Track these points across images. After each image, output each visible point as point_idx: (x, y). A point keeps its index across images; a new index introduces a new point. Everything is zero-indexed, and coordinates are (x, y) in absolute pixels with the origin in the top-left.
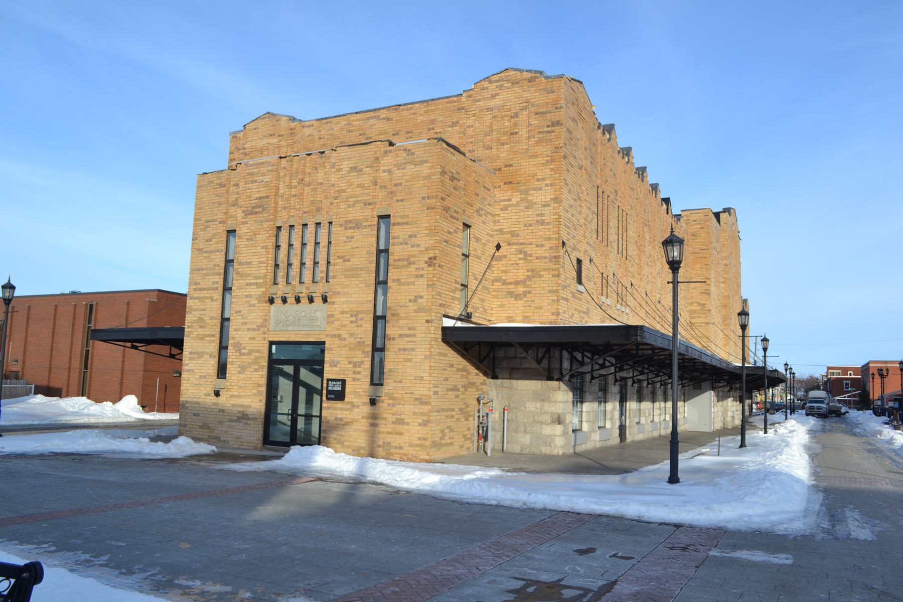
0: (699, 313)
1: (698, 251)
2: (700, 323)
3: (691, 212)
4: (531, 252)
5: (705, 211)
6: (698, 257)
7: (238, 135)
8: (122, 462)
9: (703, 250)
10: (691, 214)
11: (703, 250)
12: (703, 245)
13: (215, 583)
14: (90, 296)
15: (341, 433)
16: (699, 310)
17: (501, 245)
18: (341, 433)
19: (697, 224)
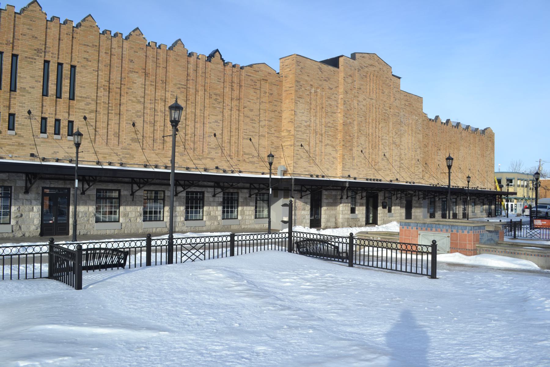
0: (287, 138)
1: (288, 89)
2: (287, 145)
3: (284, 59)
4: (23, 135)
5: (292, 56)
6: (287, 94)
7: (107, 32)
8: (77, 277)
9: (291, 87)
10: (285, 60)
11: (291, 87)
12: (290, 84)
13: (69, 241)
14: (309, 62)
15: (67, 155)
16: (287, 136)
17: (83, 119)
18: (67, 155)
19: (288, 67)
